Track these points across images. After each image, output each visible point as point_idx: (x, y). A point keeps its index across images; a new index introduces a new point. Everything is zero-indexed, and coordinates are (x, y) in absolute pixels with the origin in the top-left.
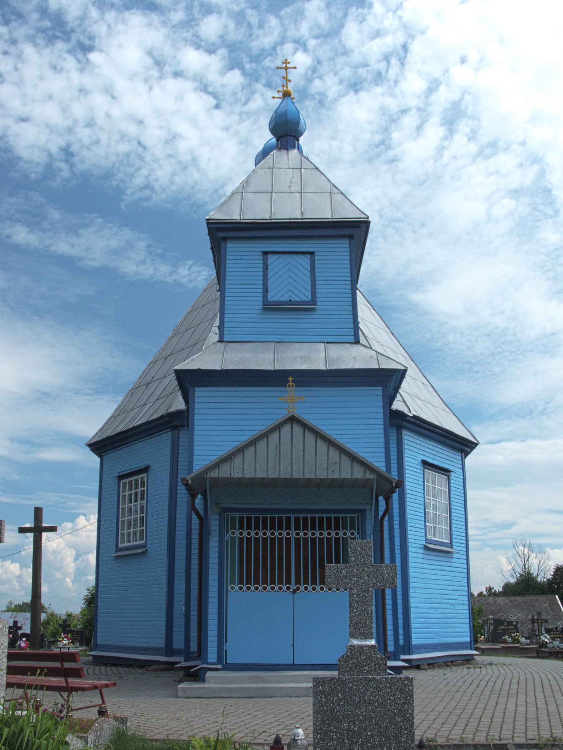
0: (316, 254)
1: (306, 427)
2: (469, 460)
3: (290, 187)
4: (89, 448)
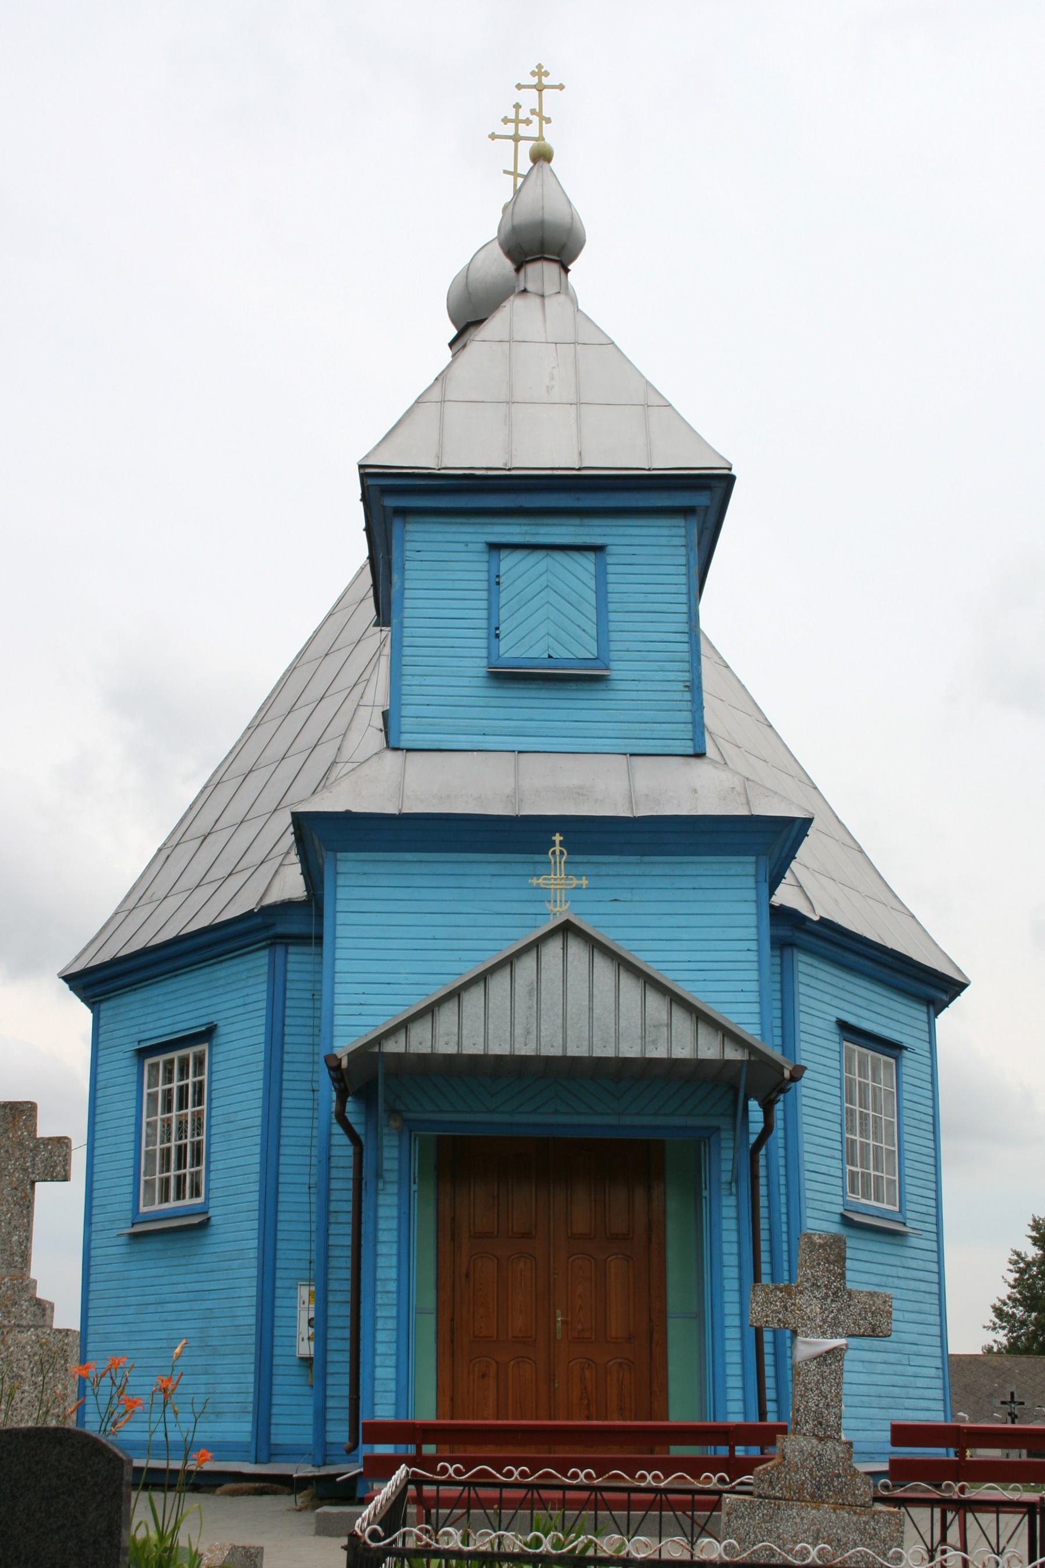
0: (610, 549)
1: (595, 945)
2: (944, 1020)
3: (549, 389)
4: (67, 986)
